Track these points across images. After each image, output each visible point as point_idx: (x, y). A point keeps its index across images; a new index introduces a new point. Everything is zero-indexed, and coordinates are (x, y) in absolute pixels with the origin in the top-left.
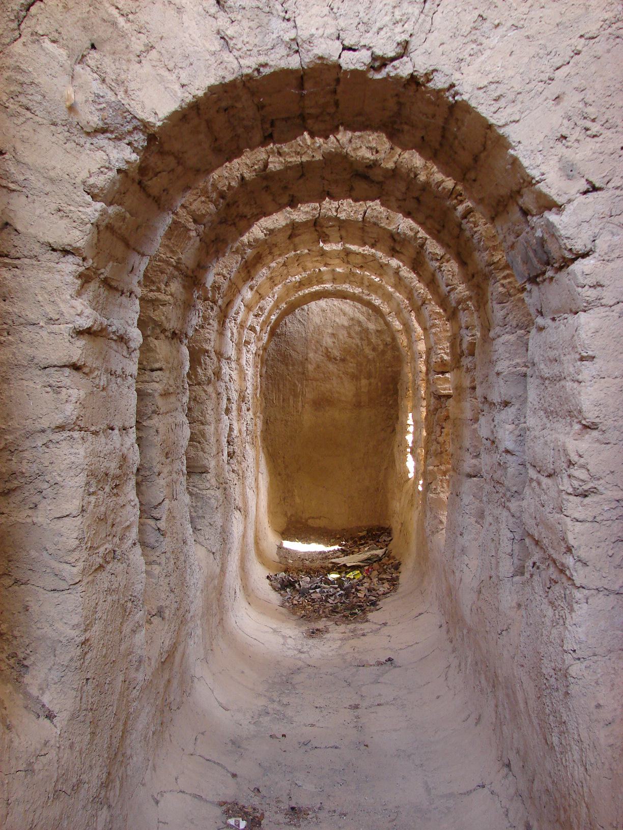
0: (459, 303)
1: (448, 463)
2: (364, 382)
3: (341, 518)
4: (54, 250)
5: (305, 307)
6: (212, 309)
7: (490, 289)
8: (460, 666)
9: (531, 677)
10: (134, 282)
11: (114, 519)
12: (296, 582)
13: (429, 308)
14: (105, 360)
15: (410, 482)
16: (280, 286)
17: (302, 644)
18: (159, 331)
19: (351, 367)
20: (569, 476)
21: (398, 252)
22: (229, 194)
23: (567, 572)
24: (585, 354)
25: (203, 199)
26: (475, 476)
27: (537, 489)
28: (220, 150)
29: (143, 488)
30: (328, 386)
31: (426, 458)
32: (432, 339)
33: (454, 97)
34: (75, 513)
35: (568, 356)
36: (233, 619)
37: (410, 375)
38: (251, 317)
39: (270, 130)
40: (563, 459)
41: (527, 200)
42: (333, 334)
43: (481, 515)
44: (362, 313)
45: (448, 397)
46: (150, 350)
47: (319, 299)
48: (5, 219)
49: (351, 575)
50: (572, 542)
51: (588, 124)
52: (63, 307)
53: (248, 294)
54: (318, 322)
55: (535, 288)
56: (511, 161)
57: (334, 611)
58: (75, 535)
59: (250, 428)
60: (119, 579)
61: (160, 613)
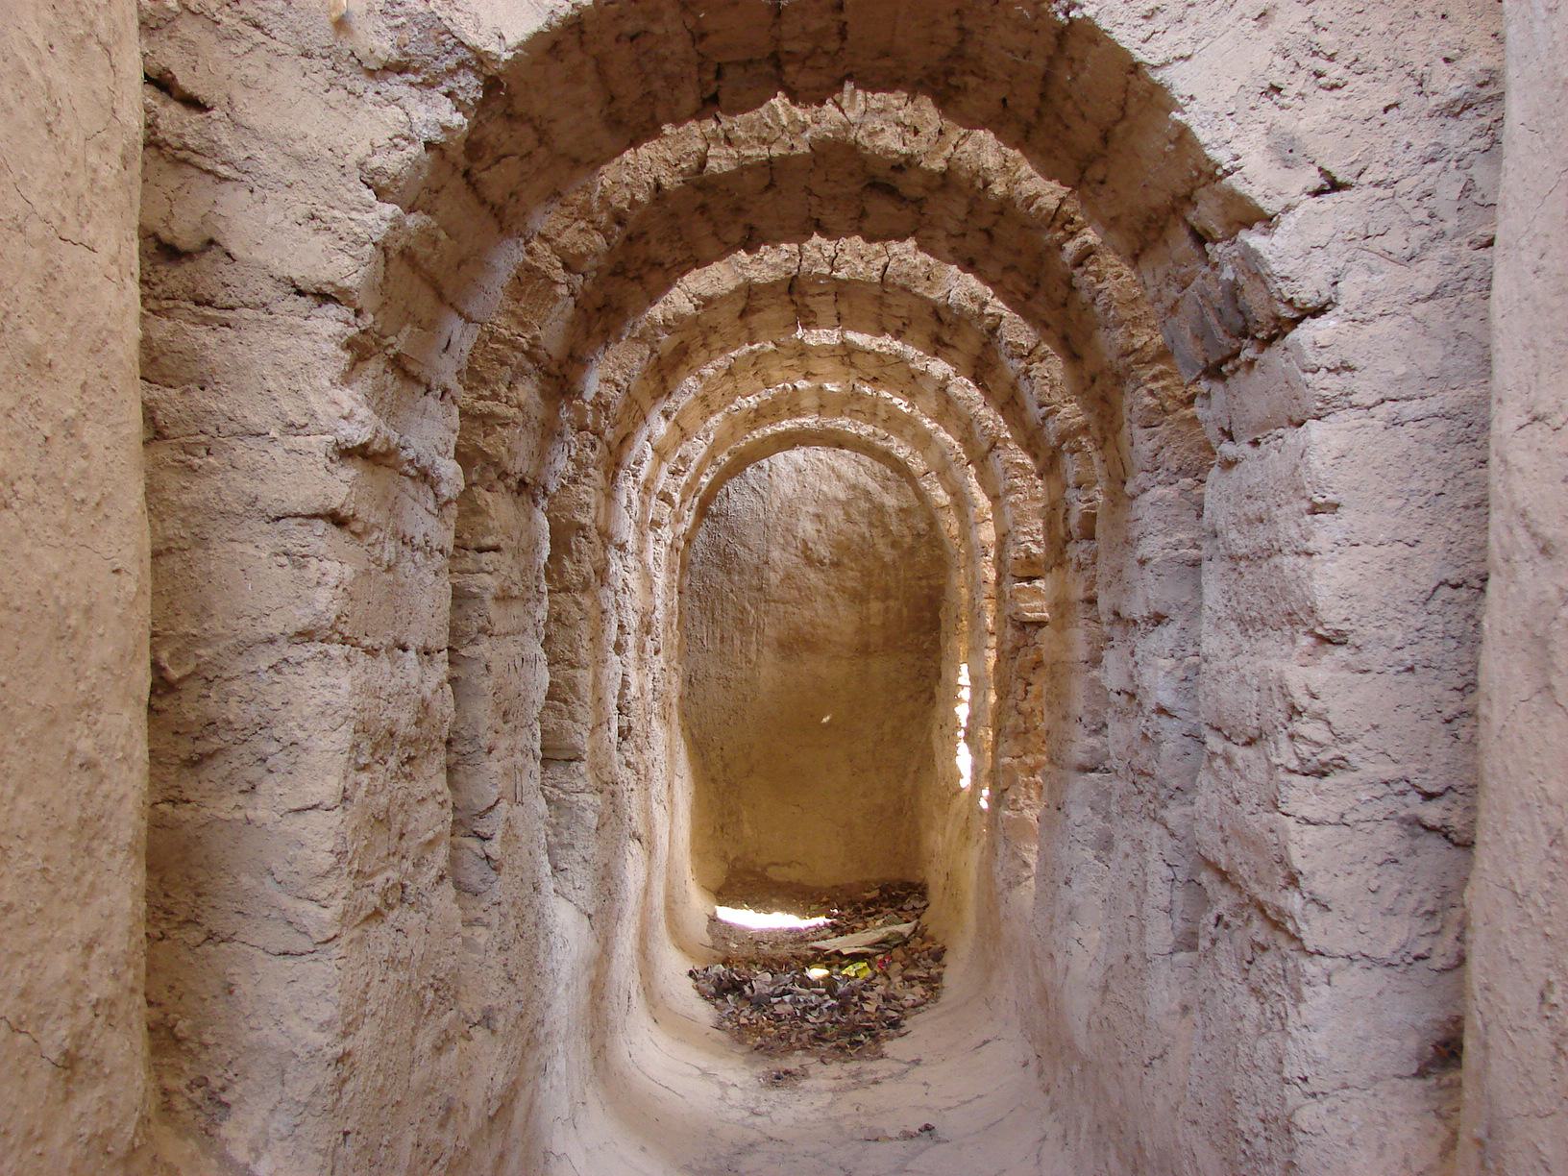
0: (1063, 438)
1: (1040, 751)
2: (875, 606)
3: (830, 866)
4: (300, 293)
5: (765, 463)
6: (593, 446)
7: (1127, 401)
8: (1065, 1136)
9: (1213, 1143)
10: (446, 370)
11: (404, 824)
12: (745, 982)
13: (1004, 456)
14: (394, 512)
15: (963, 795)
16: (719, 416)
17: (757, 1099)
18: (494, 476)
19: (852, 578)
20: (1291, 737)
21: (946, 345)
22: (632, 217)
23: (1290, 926)
24: (1321, 500)
25: (583, 224)
26: (1093, 770)
27: (1224, 771)
28: (619, 123)
29: (459, 777)
30: (807, 613)
31: (996, 743)
32: (1010, 514)
33: (1067, 14)
34: (329, 803)
35: (1286, 509)
36: (624, 1050)
37: (964, 591)
38: (664, 473)
39: (714, 86)
40: (1278, 705)
41: (1206, 213)
42: (818, 516)
43: (1106, 844)
44: (874, 476)
45: (1040, 624)
46: (477, 511)
47: (792, 447)
48: (208, 233)
49: (850, 971)
50: (1298, 863)
51: (1321, 64)
52: (317, 403)
53: (660, 428)
54: (790, 492)
55: (1217, 388)
56: (1174, 136)
57: (819, 1036)
58: (329, 845)
59: (660, 686)
60: (411, 941)
61: (487, 1020)
